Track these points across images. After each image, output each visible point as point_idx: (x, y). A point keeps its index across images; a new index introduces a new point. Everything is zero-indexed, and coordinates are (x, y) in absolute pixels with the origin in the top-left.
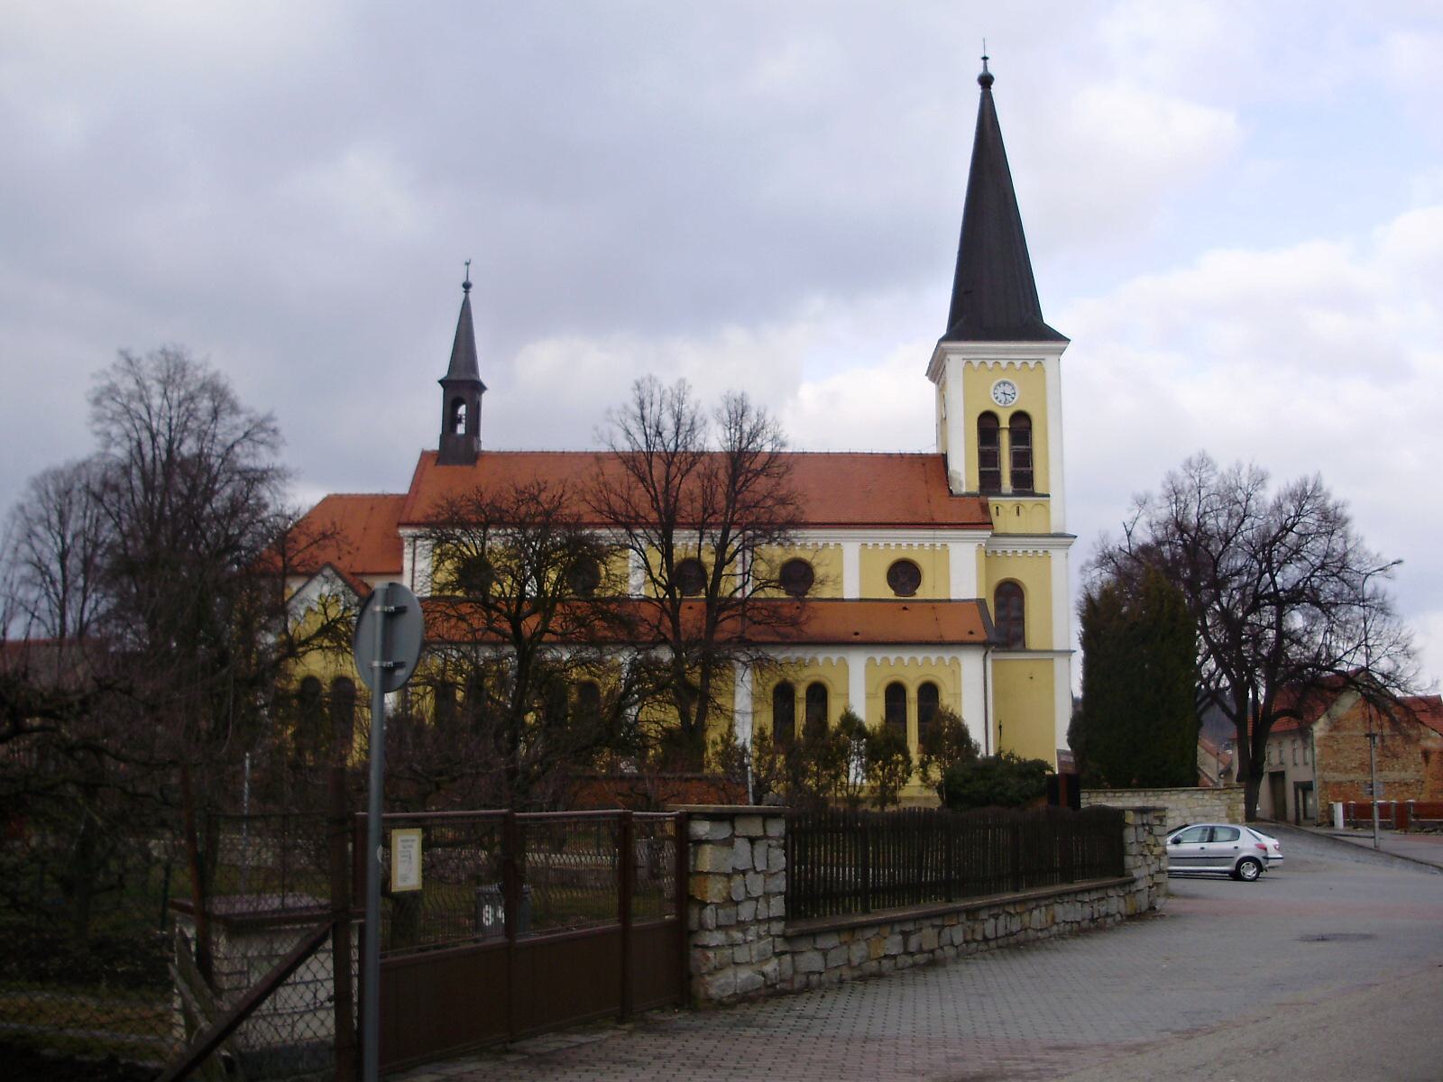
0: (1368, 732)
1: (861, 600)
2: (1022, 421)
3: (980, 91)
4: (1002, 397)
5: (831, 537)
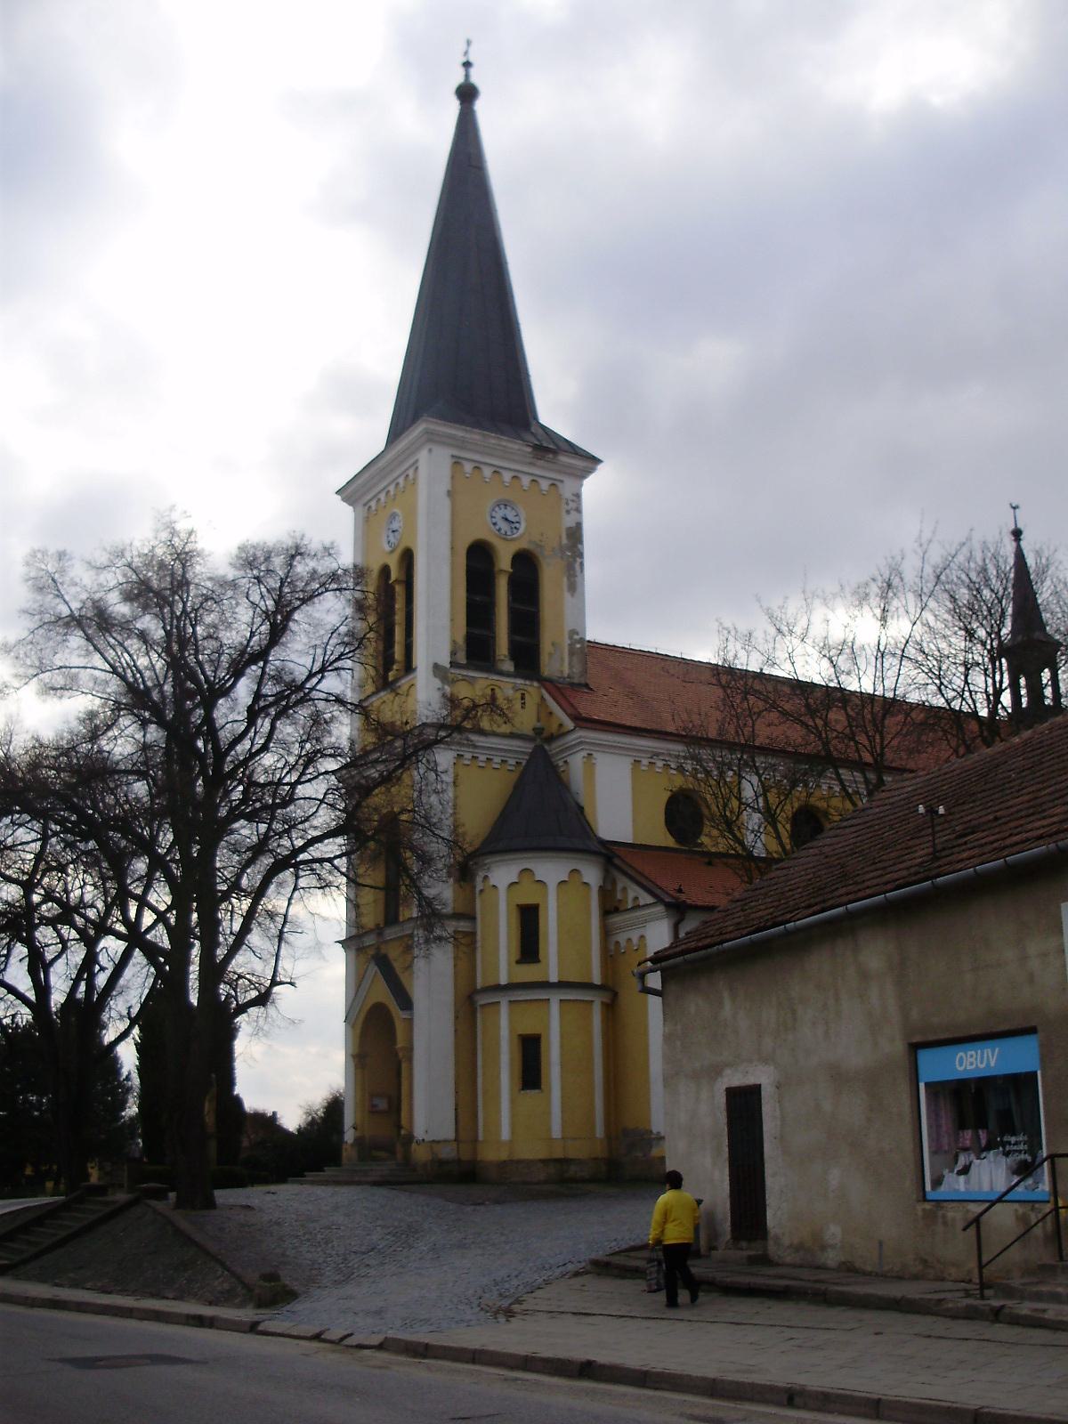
2: (526, 563)
3: (459, 107)
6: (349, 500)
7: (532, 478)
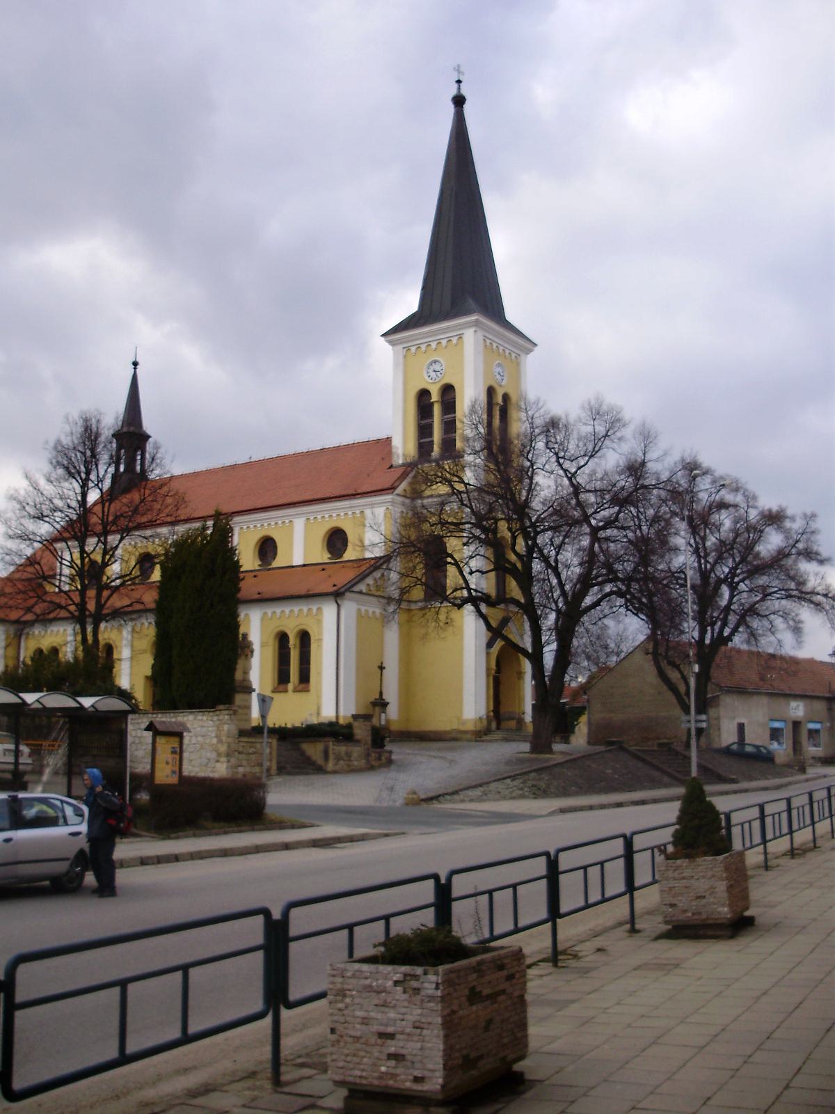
1: (304, 565)
4: (433, 375)
5: (272, 518)
6: (392, 343)
7: (426, 344)
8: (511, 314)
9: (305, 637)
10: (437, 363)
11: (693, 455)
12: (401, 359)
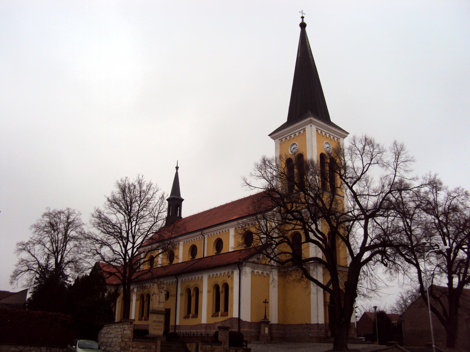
0: (160, 294)
6: (274, 138)
8: (332, 120)
9: (226, 287)
10: (295, 145)
11: (433, 177)
12: (278, 145)
